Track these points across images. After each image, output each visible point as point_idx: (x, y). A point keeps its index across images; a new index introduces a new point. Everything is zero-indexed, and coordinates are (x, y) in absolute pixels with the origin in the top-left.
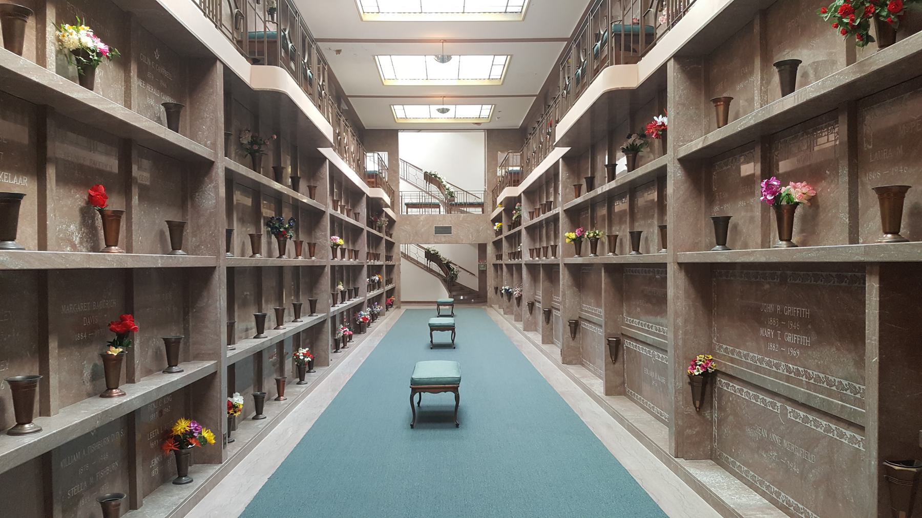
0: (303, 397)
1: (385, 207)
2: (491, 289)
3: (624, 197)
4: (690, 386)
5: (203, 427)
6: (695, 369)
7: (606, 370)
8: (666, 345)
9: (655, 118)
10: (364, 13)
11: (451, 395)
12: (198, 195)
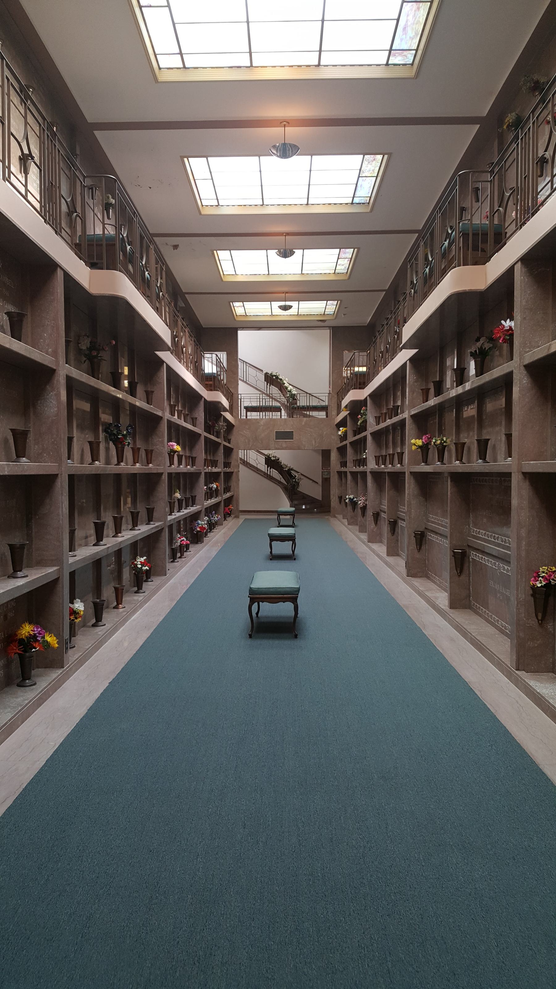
0: (141, 606)
1: (223, 412)
2: (334, 498)
3: (473, 403)
4: (533, 599)
5: (46, 632)
6: (538, 581)
7: (450, 583)
8: (509, 555)
9: (503, 322)
10: (202, 206)
11: (289, 606)
12: (41, 403)
